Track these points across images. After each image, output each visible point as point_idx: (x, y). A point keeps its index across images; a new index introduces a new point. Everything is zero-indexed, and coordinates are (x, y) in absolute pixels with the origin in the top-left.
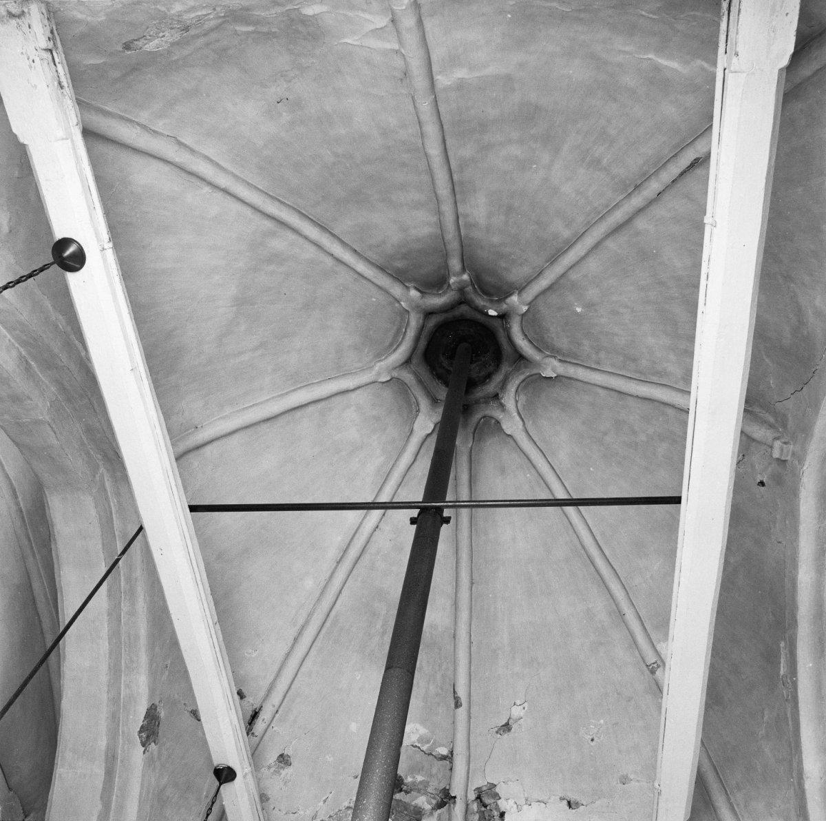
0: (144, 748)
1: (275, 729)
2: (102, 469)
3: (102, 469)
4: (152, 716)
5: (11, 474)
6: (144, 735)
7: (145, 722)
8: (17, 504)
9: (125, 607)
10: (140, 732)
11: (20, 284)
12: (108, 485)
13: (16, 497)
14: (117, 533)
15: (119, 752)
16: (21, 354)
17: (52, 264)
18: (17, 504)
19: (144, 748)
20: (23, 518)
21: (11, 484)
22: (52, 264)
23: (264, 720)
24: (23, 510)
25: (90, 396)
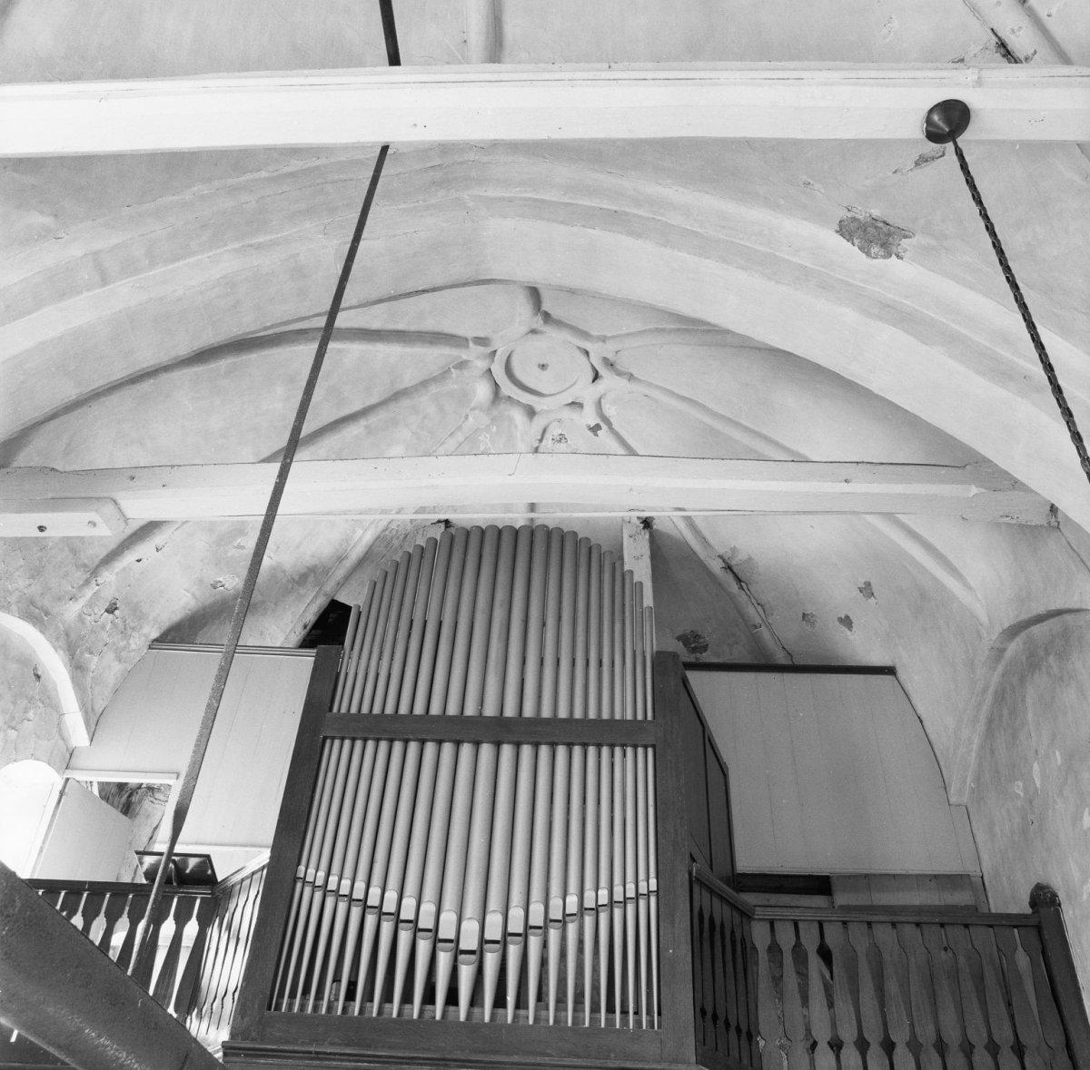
0: (894, 256)
1: (1054, 11)
2: (465, 196)
3: (465, 196)
4: (848, 229)
5: (639, 326)
6: (875, 250)
7: (856, 242)
8: (671, 331)
9: (676, 219)
10: (868, 254)
11: (996, 230)
12: (492, 192)
13: (663, 330)
14: (566, 200)
15: (891, 296)
16: (235, 250)
17: (956, 144)
18: (671, 331)
19: (894, 256)
20: (686, 330)
21: (651, 331)
22: (956, 144)
23: (1013, 31)
24: (678, 326)
25: (323, 181)
